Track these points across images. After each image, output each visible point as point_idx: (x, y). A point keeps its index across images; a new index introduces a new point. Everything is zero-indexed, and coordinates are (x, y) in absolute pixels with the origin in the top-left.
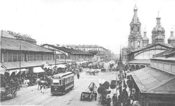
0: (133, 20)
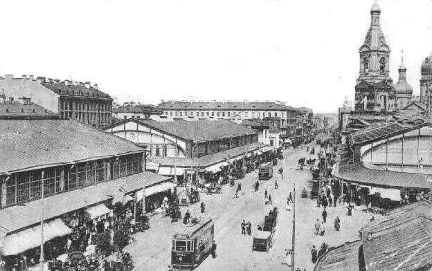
0: (369, 37)
